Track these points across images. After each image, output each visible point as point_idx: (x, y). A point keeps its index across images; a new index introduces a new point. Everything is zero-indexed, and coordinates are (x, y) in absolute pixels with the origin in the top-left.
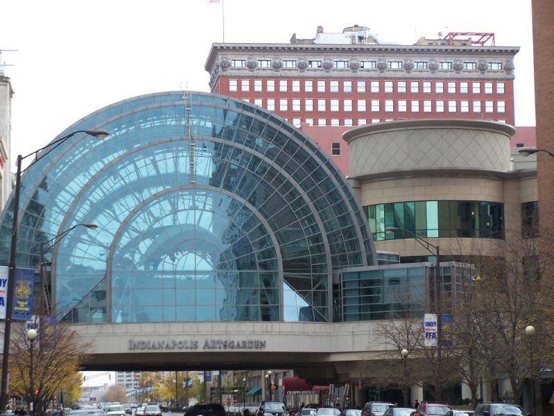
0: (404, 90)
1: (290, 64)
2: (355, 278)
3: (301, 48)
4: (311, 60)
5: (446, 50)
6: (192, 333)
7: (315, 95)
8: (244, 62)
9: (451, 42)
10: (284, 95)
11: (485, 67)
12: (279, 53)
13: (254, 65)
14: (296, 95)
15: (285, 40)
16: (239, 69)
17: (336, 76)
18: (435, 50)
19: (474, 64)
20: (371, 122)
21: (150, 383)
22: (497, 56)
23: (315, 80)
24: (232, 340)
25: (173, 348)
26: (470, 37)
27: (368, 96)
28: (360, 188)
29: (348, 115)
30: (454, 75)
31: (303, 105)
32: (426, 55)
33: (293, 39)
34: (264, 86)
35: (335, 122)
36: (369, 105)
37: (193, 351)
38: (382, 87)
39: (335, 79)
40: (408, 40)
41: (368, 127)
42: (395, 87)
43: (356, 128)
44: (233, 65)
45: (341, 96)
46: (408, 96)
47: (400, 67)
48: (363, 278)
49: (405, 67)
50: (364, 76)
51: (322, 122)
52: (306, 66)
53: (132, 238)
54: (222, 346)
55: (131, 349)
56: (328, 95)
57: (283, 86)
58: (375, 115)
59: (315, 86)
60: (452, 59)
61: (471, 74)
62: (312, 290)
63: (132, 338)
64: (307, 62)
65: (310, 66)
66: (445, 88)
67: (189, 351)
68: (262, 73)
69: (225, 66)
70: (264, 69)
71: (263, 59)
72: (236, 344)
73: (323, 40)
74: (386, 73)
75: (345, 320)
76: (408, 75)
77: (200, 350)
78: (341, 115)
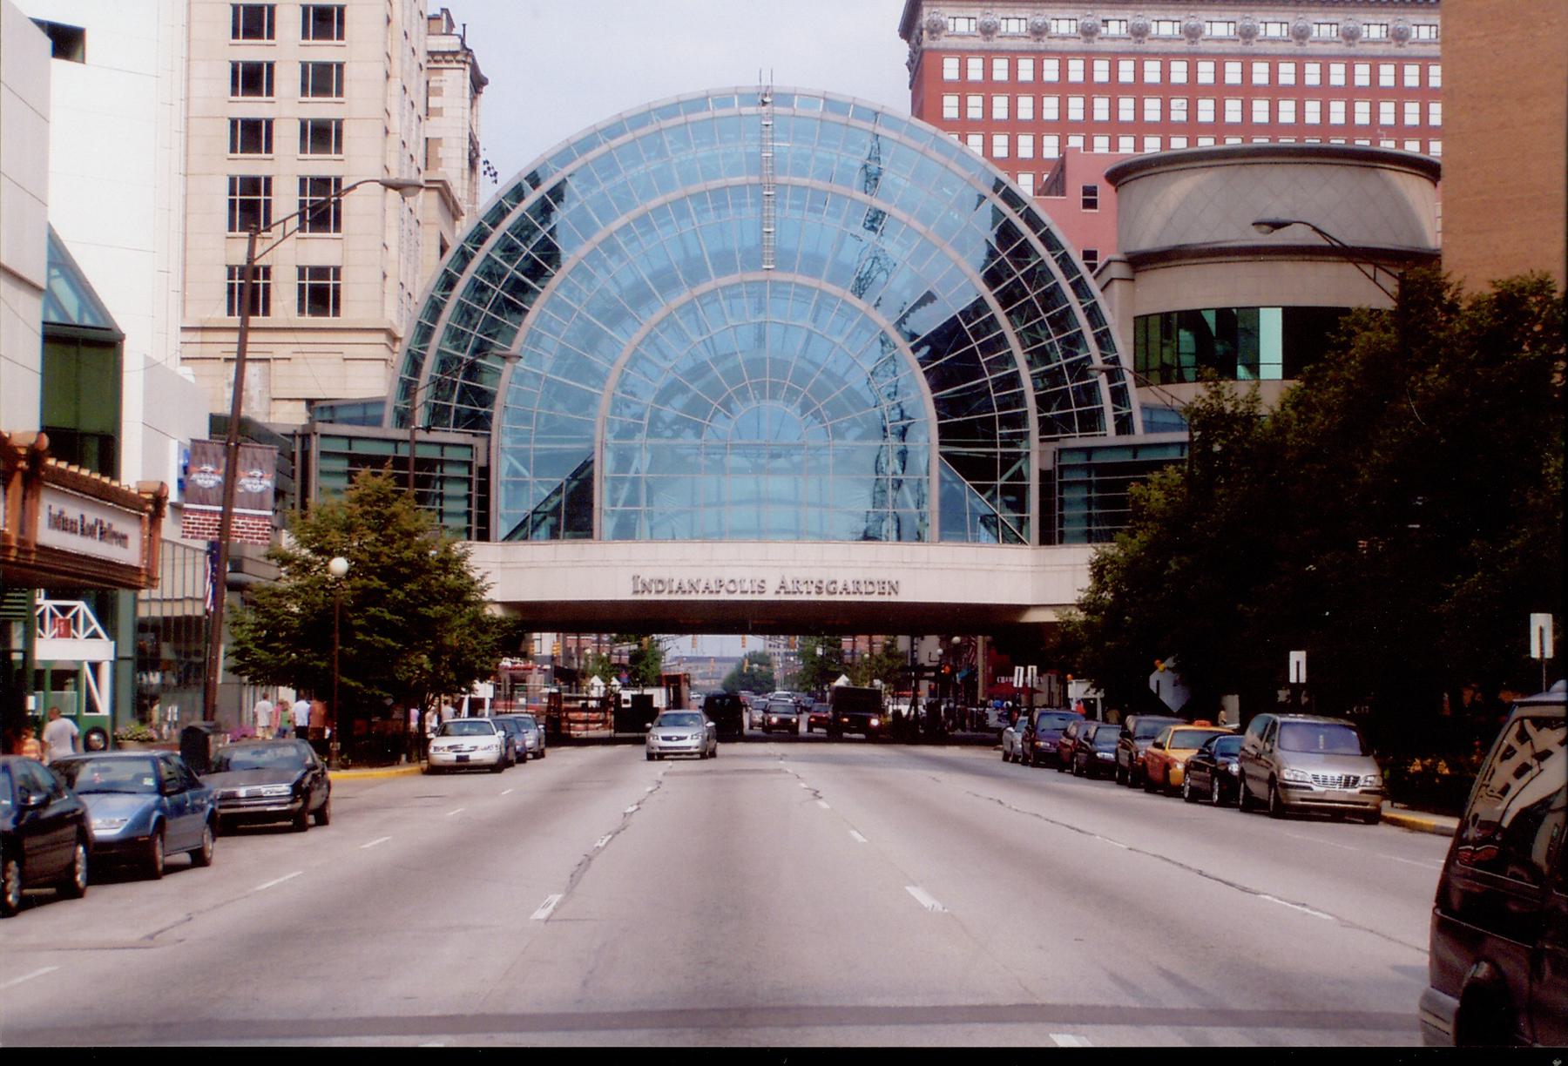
2: (1080, 460)
4: (1106, 18)
11: (1403, 35)
13: (1093, 29)
14: (1312, 92)
17: (1156, 50)
19: (1384, 28)
20: (1251, 141)
21: (516, 663)
22: (1408, 10)
23: (1114, 59)
24: (832, 579)
25: (718, 592)
27: (1220, 91)
29: (1126, 128)
30: (1393, 49)
31: (1089, 109)
34: (1114, 71)
35: (1101, 143)
37: (757, 597)
38: (1247, 74)
39: (1154, 55)
41: (1243, 149)
42: (1274, 74)
43: (1139, 156)
44: (951, 28)
45: (1113, 89)
46: (1299, 92)
52: (1098, 30)
53: (1159, 370)
54: (813, 589)
59: (1114, 71)
64: (1099, 22)
65: (1104, 30)
67: (748, 597)
68: (1007, 44)
69: (936, 29)
70: (1013, 37)
71: (1011, 15)
72: (840, 587)
74: (1201, 44)
75: (1061, 542)
76: (1299, 50)
77: (770, 596)
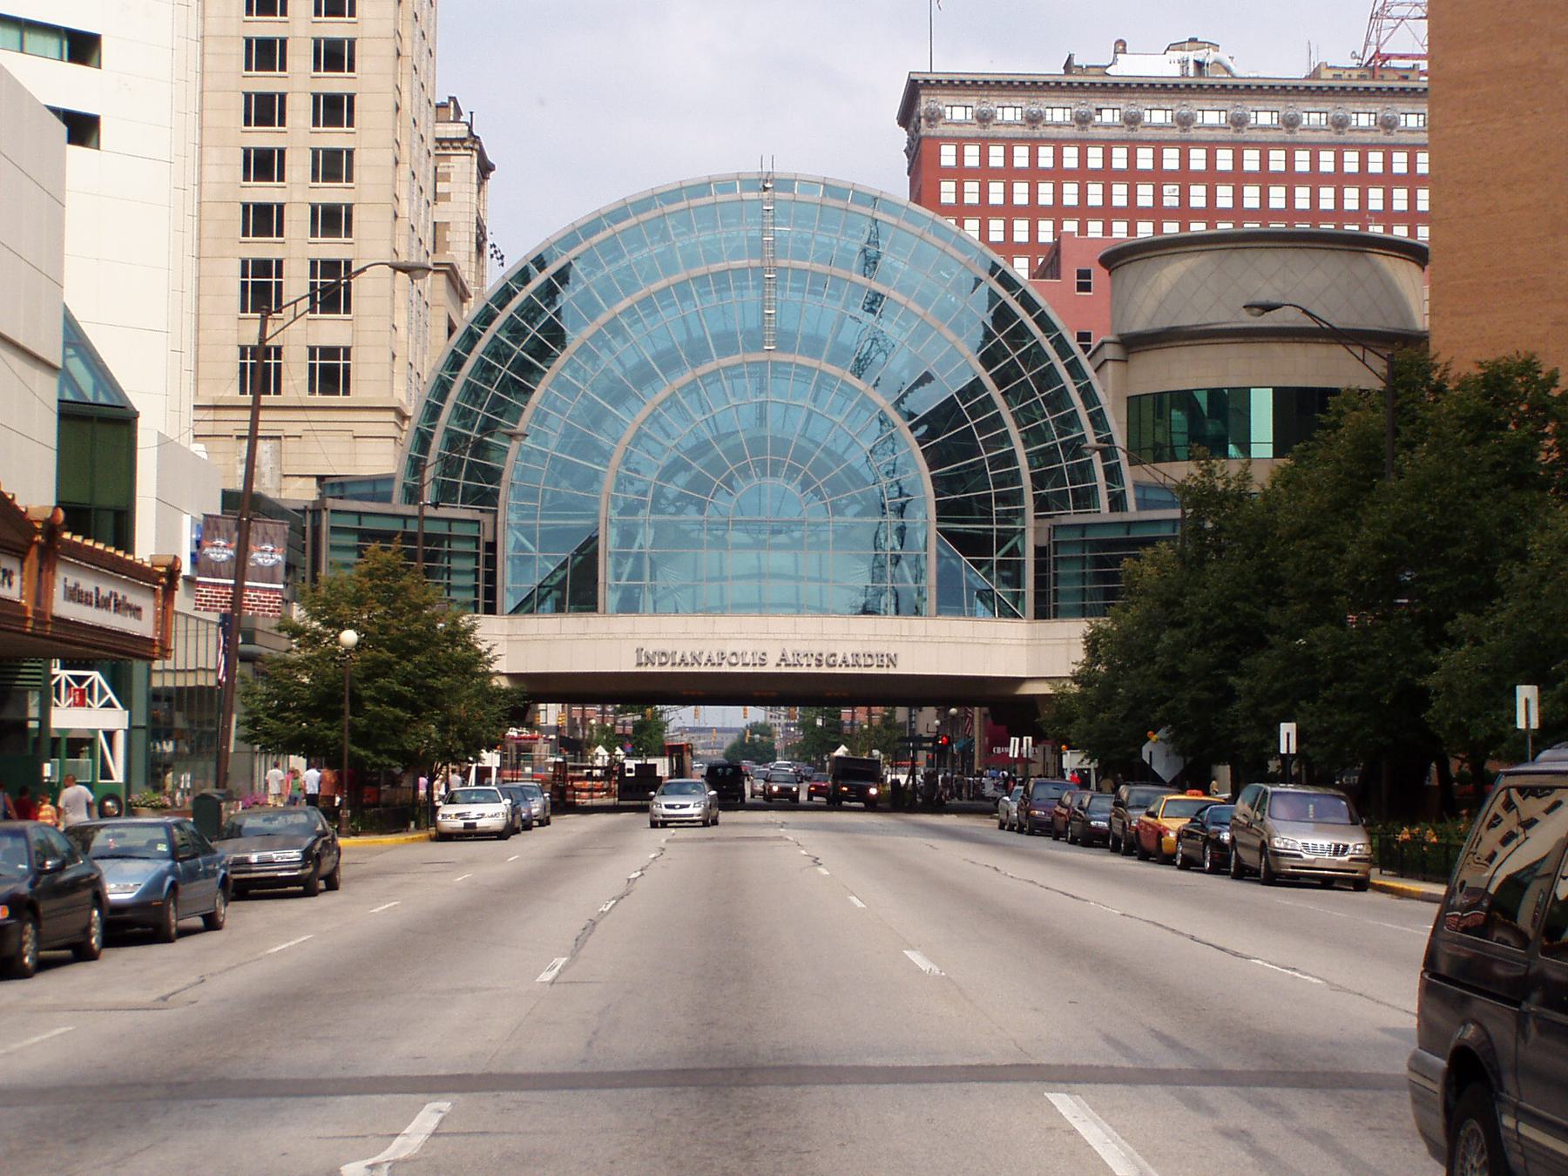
0: (1281, 167)
1: (1058, 114)
2: (1075, 536)
3: (1081, 84)
5: (1367, 89)
6: (757, 636)
7: (1107, 175)
8: (969, 110)
9: (1378, 73)
10: (1351, 179)
12: (1039, 94)
15: (1052, 68)
16: (959, 124)
17: (1149, 137)
18: (1343, 88)
24: (832, 651)
25: (720, 664)
26: (1416, 62)
28: (1127, 361)
29: (1119, 213)
30: (1381, 136)
32: (1326, 98)
33: (1068, 66)
36: (1211, 196)
37: (758, 669)
38: (1238, 160)
40: (1294, 69)
43: (1132, 240)
44: (948, 116)
47: (1275, 121)
48: (1091, 536)
49: (1284, 122)
50: (1203, 138)
51: (1095, 228)
52: (1091, 119)
54: (813, 662)
55: (639, 664)
56: (1033, 175)
57: (1351, 162)
58: (1225, 214)
59: (1158, 159)
60: (1377, 107)
61: (1268, 133)
62: (995, 558)
63: (640, 644)
65: (1098, 118)
66: (1363, 162)
68: (1003, 132)
69: (934, 117)
70: (1009, 124)
73: (1128, 67)
75: (1055, 616)
77: (770, 668)
78: (1107, 213)
